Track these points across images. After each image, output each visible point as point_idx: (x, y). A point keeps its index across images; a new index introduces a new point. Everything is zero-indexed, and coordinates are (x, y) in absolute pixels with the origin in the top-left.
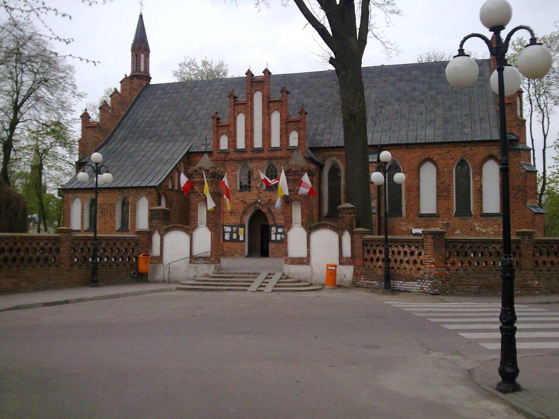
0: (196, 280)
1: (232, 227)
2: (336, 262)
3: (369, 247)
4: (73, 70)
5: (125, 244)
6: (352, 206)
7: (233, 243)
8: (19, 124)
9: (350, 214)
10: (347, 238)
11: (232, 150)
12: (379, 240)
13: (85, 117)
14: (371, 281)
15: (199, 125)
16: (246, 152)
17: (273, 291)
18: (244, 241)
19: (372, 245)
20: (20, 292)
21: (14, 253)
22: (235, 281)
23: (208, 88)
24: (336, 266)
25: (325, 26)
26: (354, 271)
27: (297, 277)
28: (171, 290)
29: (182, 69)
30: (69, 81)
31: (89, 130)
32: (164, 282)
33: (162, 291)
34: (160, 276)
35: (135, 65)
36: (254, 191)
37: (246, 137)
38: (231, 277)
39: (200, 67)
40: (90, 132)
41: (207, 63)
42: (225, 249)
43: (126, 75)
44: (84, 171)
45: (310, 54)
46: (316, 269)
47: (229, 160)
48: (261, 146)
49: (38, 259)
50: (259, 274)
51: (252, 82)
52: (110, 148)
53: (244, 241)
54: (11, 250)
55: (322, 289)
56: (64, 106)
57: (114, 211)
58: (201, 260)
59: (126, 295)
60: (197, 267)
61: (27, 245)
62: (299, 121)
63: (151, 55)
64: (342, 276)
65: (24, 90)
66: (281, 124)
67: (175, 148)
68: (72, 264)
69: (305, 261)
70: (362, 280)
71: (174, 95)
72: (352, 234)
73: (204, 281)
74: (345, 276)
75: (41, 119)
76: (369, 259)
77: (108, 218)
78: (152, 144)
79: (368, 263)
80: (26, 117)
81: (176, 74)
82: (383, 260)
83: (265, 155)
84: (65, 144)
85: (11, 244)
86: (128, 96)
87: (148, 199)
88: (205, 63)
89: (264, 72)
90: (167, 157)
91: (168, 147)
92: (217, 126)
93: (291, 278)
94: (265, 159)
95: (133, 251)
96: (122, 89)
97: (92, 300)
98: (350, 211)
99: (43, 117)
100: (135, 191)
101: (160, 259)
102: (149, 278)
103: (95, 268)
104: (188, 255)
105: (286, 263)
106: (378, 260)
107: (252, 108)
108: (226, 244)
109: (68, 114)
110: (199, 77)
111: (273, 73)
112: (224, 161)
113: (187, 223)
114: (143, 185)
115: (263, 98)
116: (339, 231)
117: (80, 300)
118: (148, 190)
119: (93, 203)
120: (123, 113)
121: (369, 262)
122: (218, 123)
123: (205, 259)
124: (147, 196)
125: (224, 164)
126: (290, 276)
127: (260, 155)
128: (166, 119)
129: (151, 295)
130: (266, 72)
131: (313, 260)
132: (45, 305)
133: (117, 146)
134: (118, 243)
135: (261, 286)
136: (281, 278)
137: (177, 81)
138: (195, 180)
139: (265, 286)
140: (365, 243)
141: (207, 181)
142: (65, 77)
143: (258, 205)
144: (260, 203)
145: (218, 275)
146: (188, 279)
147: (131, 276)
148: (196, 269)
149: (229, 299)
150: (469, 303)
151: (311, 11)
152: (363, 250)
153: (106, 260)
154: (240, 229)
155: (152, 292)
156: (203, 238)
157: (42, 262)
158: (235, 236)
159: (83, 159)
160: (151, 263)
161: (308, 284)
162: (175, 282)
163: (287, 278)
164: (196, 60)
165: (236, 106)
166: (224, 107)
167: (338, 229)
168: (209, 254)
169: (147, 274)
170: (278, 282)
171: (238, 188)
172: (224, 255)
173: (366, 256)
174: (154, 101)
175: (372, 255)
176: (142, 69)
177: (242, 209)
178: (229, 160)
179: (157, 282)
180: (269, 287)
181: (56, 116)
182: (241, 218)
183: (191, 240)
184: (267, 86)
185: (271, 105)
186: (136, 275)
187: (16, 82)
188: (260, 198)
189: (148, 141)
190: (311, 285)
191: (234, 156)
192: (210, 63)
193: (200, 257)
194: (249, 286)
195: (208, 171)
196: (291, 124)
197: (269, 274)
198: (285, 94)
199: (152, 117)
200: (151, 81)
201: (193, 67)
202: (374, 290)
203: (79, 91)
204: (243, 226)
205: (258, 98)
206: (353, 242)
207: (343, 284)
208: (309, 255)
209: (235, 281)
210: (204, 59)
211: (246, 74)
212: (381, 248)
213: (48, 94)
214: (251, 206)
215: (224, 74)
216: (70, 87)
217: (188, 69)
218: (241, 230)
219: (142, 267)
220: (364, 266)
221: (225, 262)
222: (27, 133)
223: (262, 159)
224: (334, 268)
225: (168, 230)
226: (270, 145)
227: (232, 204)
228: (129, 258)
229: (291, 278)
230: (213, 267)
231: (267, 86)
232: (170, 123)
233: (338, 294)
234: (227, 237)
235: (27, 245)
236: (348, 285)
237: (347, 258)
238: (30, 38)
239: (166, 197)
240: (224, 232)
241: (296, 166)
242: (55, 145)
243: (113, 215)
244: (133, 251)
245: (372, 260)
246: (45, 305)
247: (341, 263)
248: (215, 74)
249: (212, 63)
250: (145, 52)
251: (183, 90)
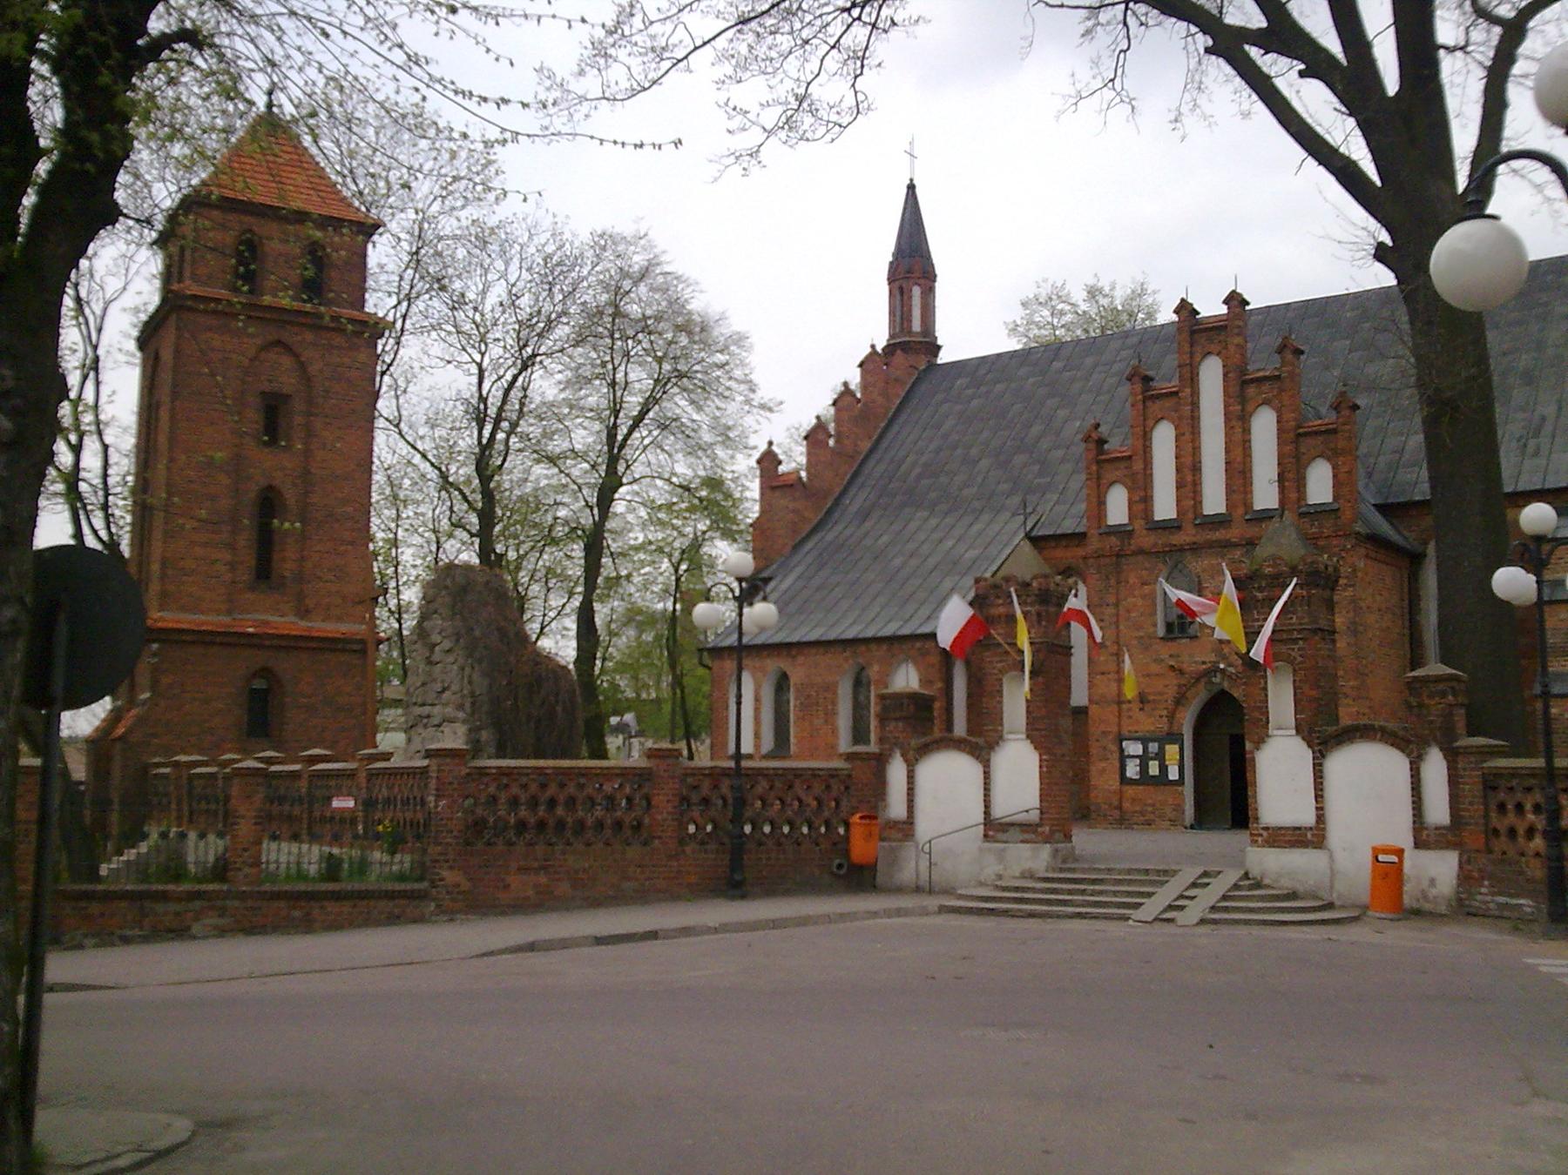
0: (997, 887)
1: (1145, 741)
2: (1405, 839)
3: (1502, 796)
4: (747, 343)
5: (818, 788)
6: (1450, 671)
7: (1151, 788)
8: (622, 490)
9: (1443, 694)
10: (1435, 767)
11: (1139, 524)
12: (1533, 773)
13: (769, 460)
14: (1511, 896)
15: (1063, 461)
16: (1179, 528)
17: (1202, 921)
18: (1181, 782)
19: (1511, 789)
20: (553, 909)
21: (542, 811)
22: (1101, 893)
23: (1089, 361)
24: (1400, 852)
25: (1354, 157)
26: (1461, 867)
27: (1287, 884)
28: (925, 912)
29: (1031, 315)
30: (738, 373)
31: (777, 493)
32: (918, 890)
33: (899, 912)
34: (907, 874)
35: (898, 319)
37: (1180, 486)
38: (1094, 882)
39: (1080, 303)
40: (782, 501)
41: (1100, 291)
42: (1126, 805)
43: (873, 346)
44: (765, 599)
45: (1304, 241)
46: (1344, 861)
47: (1135, 553)
48: (1221, 509)
49: (600, 825)
50: (1175, 872)
51: (1193, 332)
52: (830, 537)
53: (1181, 782)
54: (534, 803)
55: (1355, 919)
56: (729, 438)
57: (834, 703)
58: (1014, 833)
59: (803, 922)
60: (1003, 850)
61: (571, 789)
62: (1335, 431)
63: (940, 286)
64: (1425, 884)
65: (633, 402)
66: (1281, 442)
67: (996, 527)
68: (683, 839)
69: (1311, 837)
70: (1484, 896)
71: (999, 387)
72: (1451, 755)
73: (1017, 889)
74: (1432, 882)
75: (675, 474)
76: (1503, 831)
77: (818, 722)
78: (933, 522)
79: (1502, 843)
80: (638, 470)
81: (1014, 330)
82: (1545, 834)
83: (1233, 533)
84: (730, 535)
85: (533, 787)
86: (880, 400)
87: (918, 669)
89: (1226, 302)
90: (972, 554)
91: (977, 527)
92: (1098, 462)
93: (1268, 887)
94: (1236, 545)
95: (838, 804)
96: (865, 385)
97: (716, 930)
98: (1441, 686)
99: (681, 468)
100: (885, 647)
101: (906, 828)
102: (880, 879)
103: (737, 850)
104: (980, 818)
105: (1254, 842)
106: (1531, 832)
107: (1195, 405)
108: (1130, 791)
109: (739, 456)
110: (1079, 332)
111: (1257, 300)
112: (1118, 556)
114: (906, 631)
115: (1225, 375)
116: (1411, 745)
117: (686, 931)
118: (918, 645)
119: (782, 684)
120: (866, 445)
121: (1503, 838)
122: (1101, 451)
123: (1027, 830)
124: (916, 663)
125: (1118, 564)
126: (1266, 881)
127: (1218, 535)
128: (974, 452)
129: (871, 922)
130: (1235, 300)
132: (600, 941)
133: (848, 532)
134: (797, 783)
135: (1170, 908)
136: (1236, 887)
137: (1019, 347)
138: (995, 611)
139: (1182, 908)
140: (1491, 783)
141: (1025, 614)
142: (727, 363)
143: (1217, 680)
144: (1223, 671)
145: (1056, 875)
146: (981, 884)
147: (832, 873)
148: (1000, 856)
149: (1070, 939)
150: (1557, 962)
151: (1309, 121)
152: (1486, 805)
153: (767, 829)
154: (1168, 747)
155: (875, 914)
156: (1019, 772)
157: (608, 832)
158: (1154, 769)
159: (767, 567)
160: (882, 840)
161: (1320, 903)
162: (948, 891)
163: (1258, 885)
164: (1068, 287)
165: (1149, 404)
166: (1113, 411)
167: (1409, 742)
168: (1034, 816)
169: (873, 868)
170: (1225, 898)
171: (1161, 632)
172: (1085, 814)
173: (1502, 824)
174: (946, 407)
175: (1511, 818)
176: (916, 326)
177: (1171, 692)
178: (1135, 553)
179: (899, 890)
180: (1194, 911)
181: (708, 463)
182: (1171, 717)
183: (987, 775)
184: (1238, 340)
185: (1251, 390)
186: (842, 872)
187: (613, 384)
188: (1224, 658)
189: (926, 514)
190: (1330, 906)
191: (1146, 540)
192: (1107, 290)
193: (1012, 824)
194: (1138, 906)
195: (1028, 585)
196: (1310, 441)
197: (1205, 874)
198: (1289, 356)
199: (938, 450)
200: (941, 354)
201: (1060, 307)
202: (1519, 924)
203: (763, 395)
204: (1175, 738)
205: (1211, 375)
206: (1453, 780)
207: (1427, 906)
209: (1101, 893)
210: (1091, 282)
211: (1176, 312)
212: (1538, 797)
213: (689, 409)
214: (1198, 680)
215: (1150, 315)
216: (743, 387)
217: (1046, 313)
218: (1172, 750)
219: (860, 849)
220: (1490, 852)
221: (1086, 840)
222: (643, 513)
223: (1227, 545)
224: (1394, 859)
225: (925, 750)
226: (1248, 505)
227: (1143, 674)
228: (827, 823)
229: (1268, 887)
230: (1046, 851)
231: (1238, 340)
232: (985, 463)
233: (1402, 937)
234: (1132, 770)
235: (571, 789)
236: (1443, 909)
237: (1437, 828)
238: (644, 274)
239: (968, 663)
240: (1123, 758)
241: (1275, 559)
242: (712, 539)
243: (830, 715)
244: (838, 804)
245: (1512, 832)
246: (600, 941)
247: (1419, 844)
248: (1125, 317)
249: (1113, 288)
250: (922, 281)
251: (1023, 371)
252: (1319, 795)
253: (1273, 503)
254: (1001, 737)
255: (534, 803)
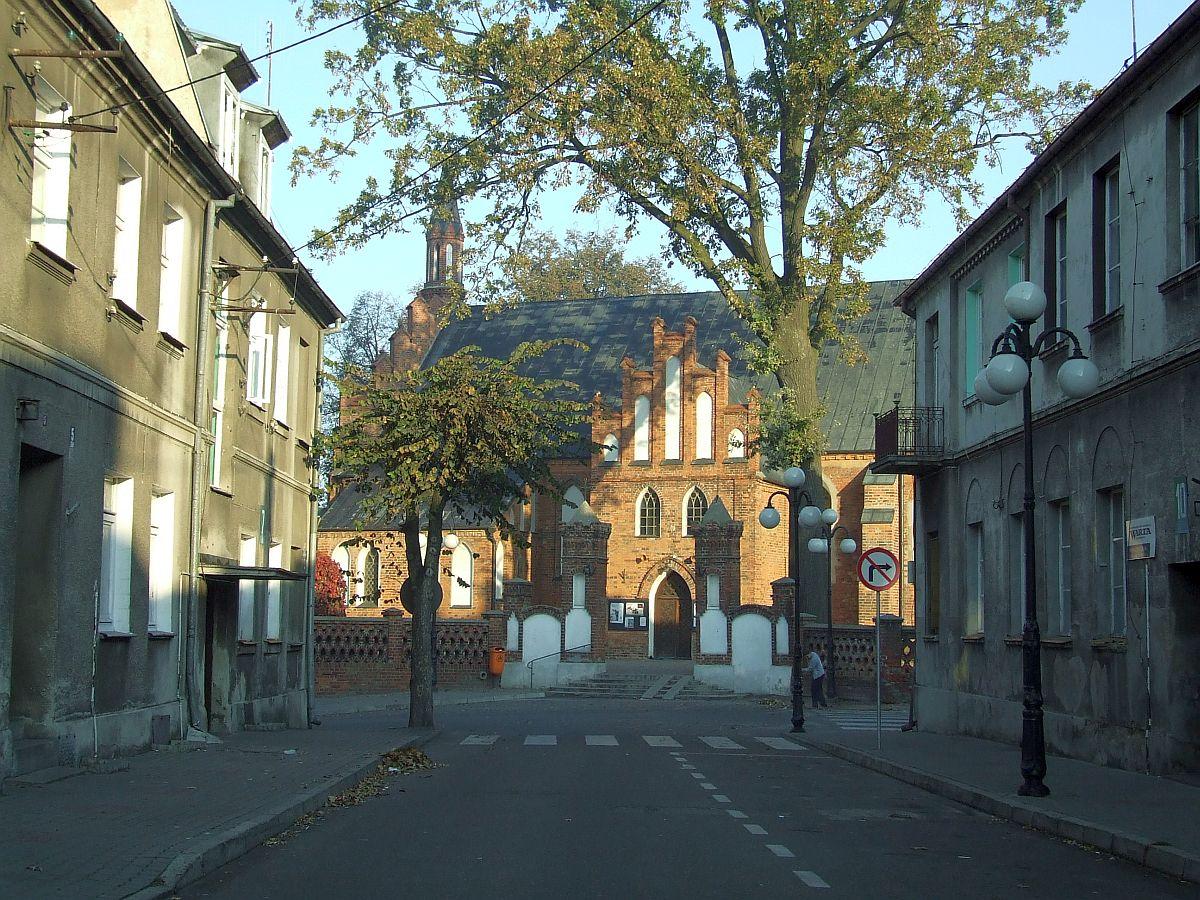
21: (362, 644)
36: (665, 538)
49: (362, 652)
60: (571, 666)
69: (725, 659)
83: (685, 472)
88: (572, 237)
101: (517, 655)
113: (559, 608)
131: (735, 661)
171: (638, 533)
186: (485, 678)
208: (730, 650)
210: (571, 228)
225: (529, 614)
252: (729, 639)
253: (708, 455)
254: (571, 608)
255: (329, 639)
